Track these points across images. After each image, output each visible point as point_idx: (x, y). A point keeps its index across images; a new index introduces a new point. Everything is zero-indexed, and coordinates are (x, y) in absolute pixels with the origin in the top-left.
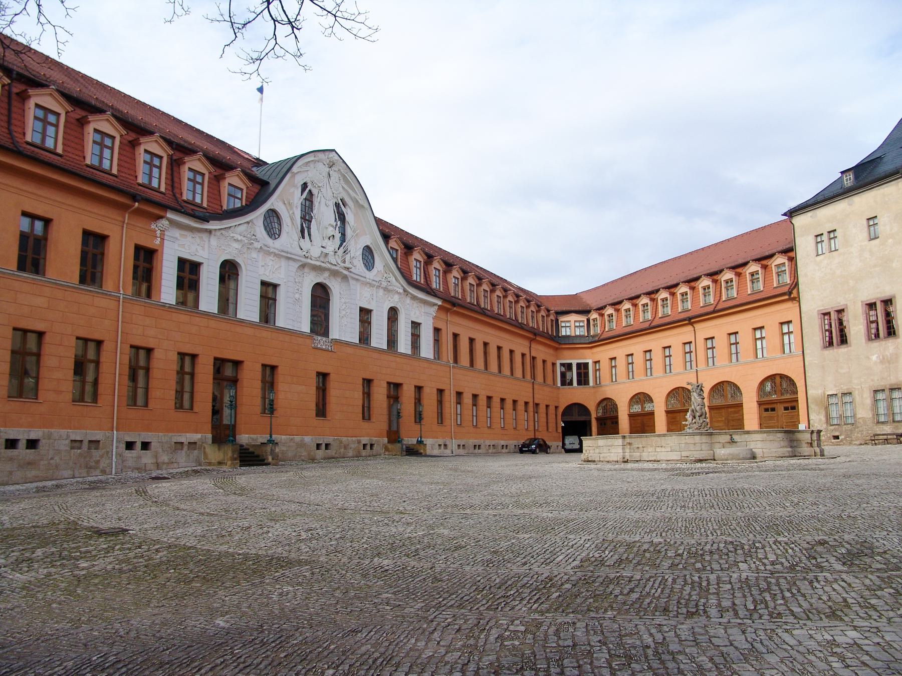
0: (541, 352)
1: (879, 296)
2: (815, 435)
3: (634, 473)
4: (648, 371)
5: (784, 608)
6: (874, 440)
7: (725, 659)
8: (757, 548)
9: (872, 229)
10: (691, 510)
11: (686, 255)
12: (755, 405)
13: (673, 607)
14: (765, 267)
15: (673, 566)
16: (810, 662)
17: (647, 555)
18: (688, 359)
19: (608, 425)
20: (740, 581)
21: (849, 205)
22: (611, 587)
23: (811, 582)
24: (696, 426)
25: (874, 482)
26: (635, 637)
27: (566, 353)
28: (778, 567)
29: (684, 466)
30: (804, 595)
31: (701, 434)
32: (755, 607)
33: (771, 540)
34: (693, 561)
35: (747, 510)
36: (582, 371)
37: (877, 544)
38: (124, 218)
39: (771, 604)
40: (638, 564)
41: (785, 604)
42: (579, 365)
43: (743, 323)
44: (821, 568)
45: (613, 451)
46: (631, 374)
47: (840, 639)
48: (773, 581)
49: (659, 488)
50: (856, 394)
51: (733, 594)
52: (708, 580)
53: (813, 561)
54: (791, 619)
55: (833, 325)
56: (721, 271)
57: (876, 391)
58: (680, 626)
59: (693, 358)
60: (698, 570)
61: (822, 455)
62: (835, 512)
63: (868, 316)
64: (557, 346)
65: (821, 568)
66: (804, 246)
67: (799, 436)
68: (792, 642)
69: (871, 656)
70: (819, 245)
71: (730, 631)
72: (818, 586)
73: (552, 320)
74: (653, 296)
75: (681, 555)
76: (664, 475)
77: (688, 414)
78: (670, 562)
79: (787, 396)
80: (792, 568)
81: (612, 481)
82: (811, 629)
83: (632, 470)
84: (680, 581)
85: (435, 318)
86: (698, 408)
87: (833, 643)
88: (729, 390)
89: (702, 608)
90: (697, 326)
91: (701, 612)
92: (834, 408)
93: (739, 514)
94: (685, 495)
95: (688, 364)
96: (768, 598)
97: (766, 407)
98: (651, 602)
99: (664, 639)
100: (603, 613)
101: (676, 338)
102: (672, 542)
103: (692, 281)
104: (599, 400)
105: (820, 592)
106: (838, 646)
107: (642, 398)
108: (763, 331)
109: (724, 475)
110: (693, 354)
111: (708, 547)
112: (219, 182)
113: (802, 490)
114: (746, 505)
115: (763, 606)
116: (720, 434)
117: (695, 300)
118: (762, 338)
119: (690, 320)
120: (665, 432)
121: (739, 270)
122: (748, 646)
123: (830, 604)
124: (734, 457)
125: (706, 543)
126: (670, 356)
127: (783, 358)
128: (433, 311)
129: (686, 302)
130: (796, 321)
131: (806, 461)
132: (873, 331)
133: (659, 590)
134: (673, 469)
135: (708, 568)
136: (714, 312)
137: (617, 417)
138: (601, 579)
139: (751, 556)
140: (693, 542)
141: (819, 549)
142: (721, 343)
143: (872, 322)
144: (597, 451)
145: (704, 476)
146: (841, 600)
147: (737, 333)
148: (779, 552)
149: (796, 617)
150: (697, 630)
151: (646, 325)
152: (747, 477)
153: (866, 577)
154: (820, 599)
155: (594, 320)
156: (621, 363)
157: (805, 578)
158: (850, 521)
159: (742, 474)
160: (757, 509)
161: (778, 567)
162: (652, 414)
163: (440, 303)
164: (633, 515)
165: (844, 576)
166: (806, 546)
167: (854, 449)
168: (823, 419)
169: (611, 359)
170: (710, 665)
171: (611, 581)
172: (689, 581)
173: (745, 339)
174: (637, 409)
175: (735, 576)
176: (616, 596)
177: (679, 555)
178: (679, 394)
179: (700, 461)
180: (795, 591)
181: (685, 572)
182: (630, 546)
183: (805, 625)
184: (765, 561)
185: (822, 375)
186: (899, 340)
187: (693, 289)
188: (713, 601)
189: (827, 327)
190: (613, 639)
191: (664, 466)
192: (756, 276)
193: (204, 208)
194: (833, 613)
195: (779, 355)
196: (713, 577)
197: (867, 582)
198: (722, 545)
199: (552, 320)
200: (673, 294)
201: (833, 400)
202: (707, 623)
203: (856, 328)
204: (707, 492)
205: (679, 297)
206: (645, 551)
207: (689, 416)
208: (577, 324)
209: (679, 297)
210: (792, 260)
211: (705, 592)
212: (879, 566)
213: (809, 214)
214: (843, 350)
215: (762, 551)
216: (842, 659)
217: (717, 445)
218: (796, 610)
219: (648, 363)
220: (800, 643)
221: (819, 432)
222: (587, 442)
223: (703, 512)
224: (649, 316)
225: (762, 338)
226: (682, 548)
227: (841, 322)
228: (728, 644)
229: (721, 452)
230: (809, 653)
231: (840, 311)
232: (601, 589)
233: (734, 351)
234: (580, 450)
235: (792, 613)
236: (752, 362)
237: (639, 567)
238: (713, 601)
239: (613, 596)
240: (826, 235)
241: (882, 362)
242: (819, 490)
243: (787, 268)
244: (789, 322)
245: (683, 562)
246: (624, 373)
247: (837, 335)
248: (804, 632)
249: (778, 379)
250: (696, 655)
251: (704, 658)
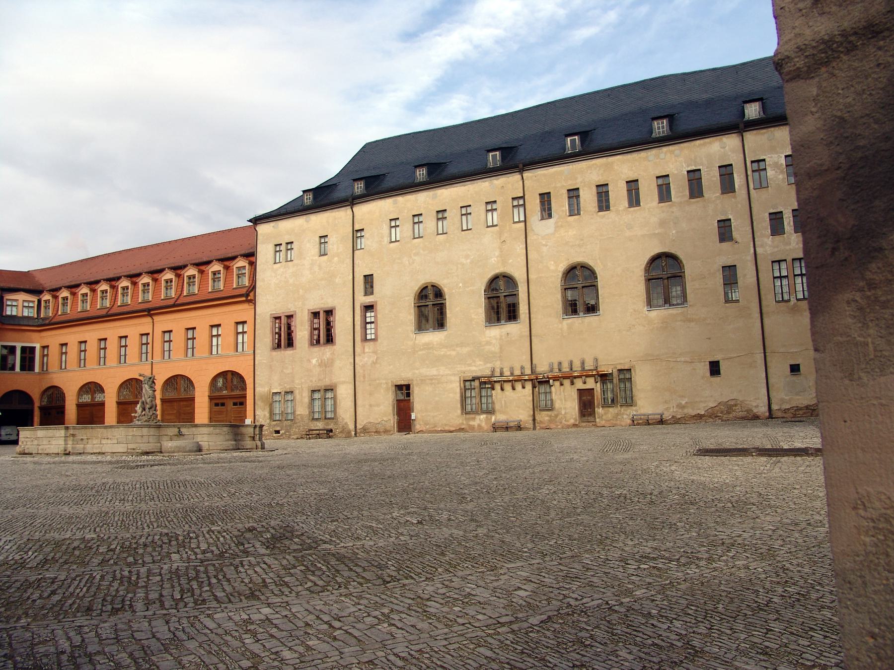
1: (322, 306)
2: (257, 429)
3: (75, 466)
4: (102, 360)
5: (209, 593)
6: (309, 434)
7: (145, 653)
8: (191, 538)
9: (323, 246)
10: (130, 503)
11: (152, 246)
12: (207, 399)
13: (97, 606)
14: (227, 268)
15: (103, 562)
16: (226, 643)
17: (77, 553)
18: (144, 351)
19: (53, 413)
20: (170, 572)
21: (307, 222)
22: (30, 590)
23: (236, 567)
24: (145, 418)
25: (302, 472)
26: (50, 643)
27: (10, 334)
28: (209, 555)
29: (130, 458)
30: (228, 580)
31: (149, 427)
32: (182, 596)
33: (205, 530)
34: (125, 555)
35: (186, 502)
36: (28, 355)
37: (297, 527)
39: (197, 592)
40: (66, 563)
41: (210, 591)
42: (24, 349)
43: (201, 319)
44: (246, 553)
45: (54, 442)
46: (82, 362)
47: (255, 617)
48: (202, 569)
49: (99, 482)
50: (297, 392)
51: (161, 586)
52: (138, 574)
53: (241, 548)
54: (214, 604)
56: (185, 266)
57: (313, 391)
58: (102, 625)
59: (150, 350)
60: (129, 565)
61: (263, 448)
62: (266, 501)
63: (312, 323)
65: (246, 553)
66: (264, 253)
67: (244, 430)
68: (212, 625)
69: (278, 628)
70: (278, 254)
71: (154, 623)
72: (243, 570)
74: (113, 283)
75: (113, 550)
76: (108, 468)
77: (139, 406)
78: (101, 558)
79: (237, 392)
80: (221, 555)
81: (49, 475)
82: (231, 611)
83: (74, 462)
84: (109, 578)
86: (148, 400)
87: (249, 621)
88: (182, 384)
89: (128, 603)
90: (156, 318)
91: (127, 607)
93: (178, 505)
94: (126, 488)
95: (144, 356)
96: (195, 586)
97: (216, 401)
98: (74, 603)
99: (83, 641)
100: (15, 622)
101: (133, 328)
102: (105, 538)
103: (155, 273)
104: (42, 389)
105: (243, 575)
106: (252, 623)
107: (93, 388)
108: (220, 329)
109: (169, 467)
110: (150, 346)
111: (143, 539)
113: (240, 481)
114: (185, 497)
115: (189, 594)
116: (168, 427)
117: (156, 291)
118: (218, 336)
119: (150, 312)
120: (115, 424)
121: (203, 268)
122: (171, 636)
123: (250, 585)
124: (179, 450)
125: (141, 536)
126: (126, 346)
129: (147, 293)
131: (248, 454)
132: (316, 337)
133: (85, 589)
134: (117, 462)
135: (140, 561)
136: (174, 306)
137: (64, 407)
138: (18, 584)
139: (184, 547)
140: (128, 535)
141: (248, 535)
142: (178, 337)
143: (315, 329)
144: (36, 442)
145: (148, 468)
146: (261, 581)
147: (194, 328)
148: (211, 541)
149: (218, 602)
150: (120, 626)
151: (104, 312)
152: (190, 469)
153: (284, 558)
154: (242, 582)
155: (46, 301)
156: (73, 350)
157: (231, 564)
158: (278, 509)
159: (186, 467)
160: (196, 500)
161: (209, 555)
162: (102, 404)
164: (66, 510)
165: (266, 559)
166: (236, 533)
167: (292, 442)
168: (268, 415)
169: (62, 345)
170: (129, 661)
171: (30, 585)
172: (118, 576)
173: (202, 335)
174: (86, 399)
175: (166, 567)
176: (34, 601)
177: (111, 550)
178: (132, 386)
179: (147, 453)
180: (220, 577)
181: (115, 568)
182: (58, 544)
183: (226, 608)
184: (197, 550)
185: (272, 375)
186: (335, 347)
187: (155, 280)
188: (141, 594)
190: (23, 650)
191: (109, 458)
192: (217, 276)
194: (252, 593)
195: (232, 353)
196: (143, 570)
197: (285, 562)
198: (157, 537)
200: (135, 284)
201: (277, 398)
202: (131, 618)
203: (302, 333)
204: (149, 485)
205: (141, 287)
206: (74, 549)
207: (138, 408)
208: (26, 304)
209: (141, 287)
210: (253, 264)
211: (133, 586)
212: (296, 547)
213: (272, 224)
214: (289, 352)
215: (195, 541)
216: (254, 634)
217: (165, 438)
218: (220, 594)
219: (102, 351)
220: (219, 625)
221: (261, 426)
222: (25, 434)
223: (143, 505)
224: (107, 304)
225: (218, 336)
226: (116, 542)
227: (289, 327)
228: (151, 636)
229: (168, 445)
230: (226, 633)
231: (290, 317)
232: (17, 594)
233: (190, 346)
234: (16, 442)
235: (216, 599)
237: (66, 566)
238: (141, 594)
239: (30, 601)
240: (284, 245)
241: (320, 365)
242: (255, 481)
243: (247, 271)
244: (244, 323)
245: (115, 557)
246: (76, 361)
247: (285, 338)
248: (224, 615)
249: (229, 376)
250: (115, 653)
251: (124, 655)
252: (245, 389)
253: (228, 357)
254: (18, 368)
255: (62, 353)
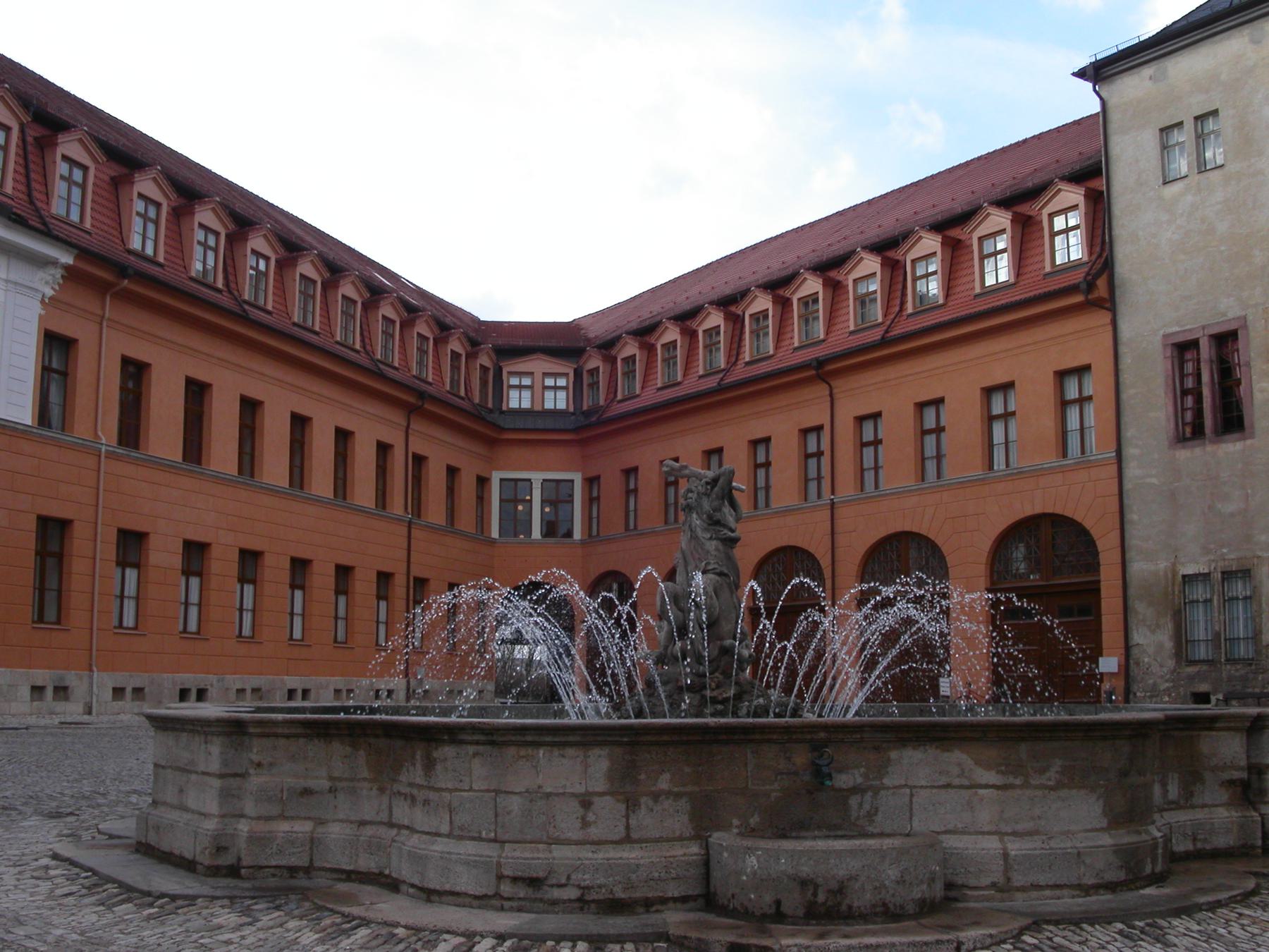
0: (441, 448)
18: (812, 473)
21: (1256, 42)
38: (103, 308)
55: (1205, 378)
59: (826, 471)
64: (494, 435)
66: (1132, 157)
73: (484, 369)
85: (50, 304)
90: (840, 385)
92: (1200, 613)
95: (813, 486)
110: (825, 460)
112: (42, 150)
118: (1007, 415)
119: (823, 370)
127: (1062, 470)
128: (46, 283)
130: (1102, 367)
132: (1189, 416)
163: (67, 259)
168: (1169, 645)
169: (755, 443)
189: (1190, 383)
193: (161, 265)
195: (1052, 460)
199: (484, 369)
201: (1199, 592)
213: (1147, 71)
214: (1231, 448)
225: (1007, 415)
236: (982, 481)
240: (1189, 125)
252: (1094, 567)
253: (654, 533)
254: (536, 533)
255: (757, 466)
